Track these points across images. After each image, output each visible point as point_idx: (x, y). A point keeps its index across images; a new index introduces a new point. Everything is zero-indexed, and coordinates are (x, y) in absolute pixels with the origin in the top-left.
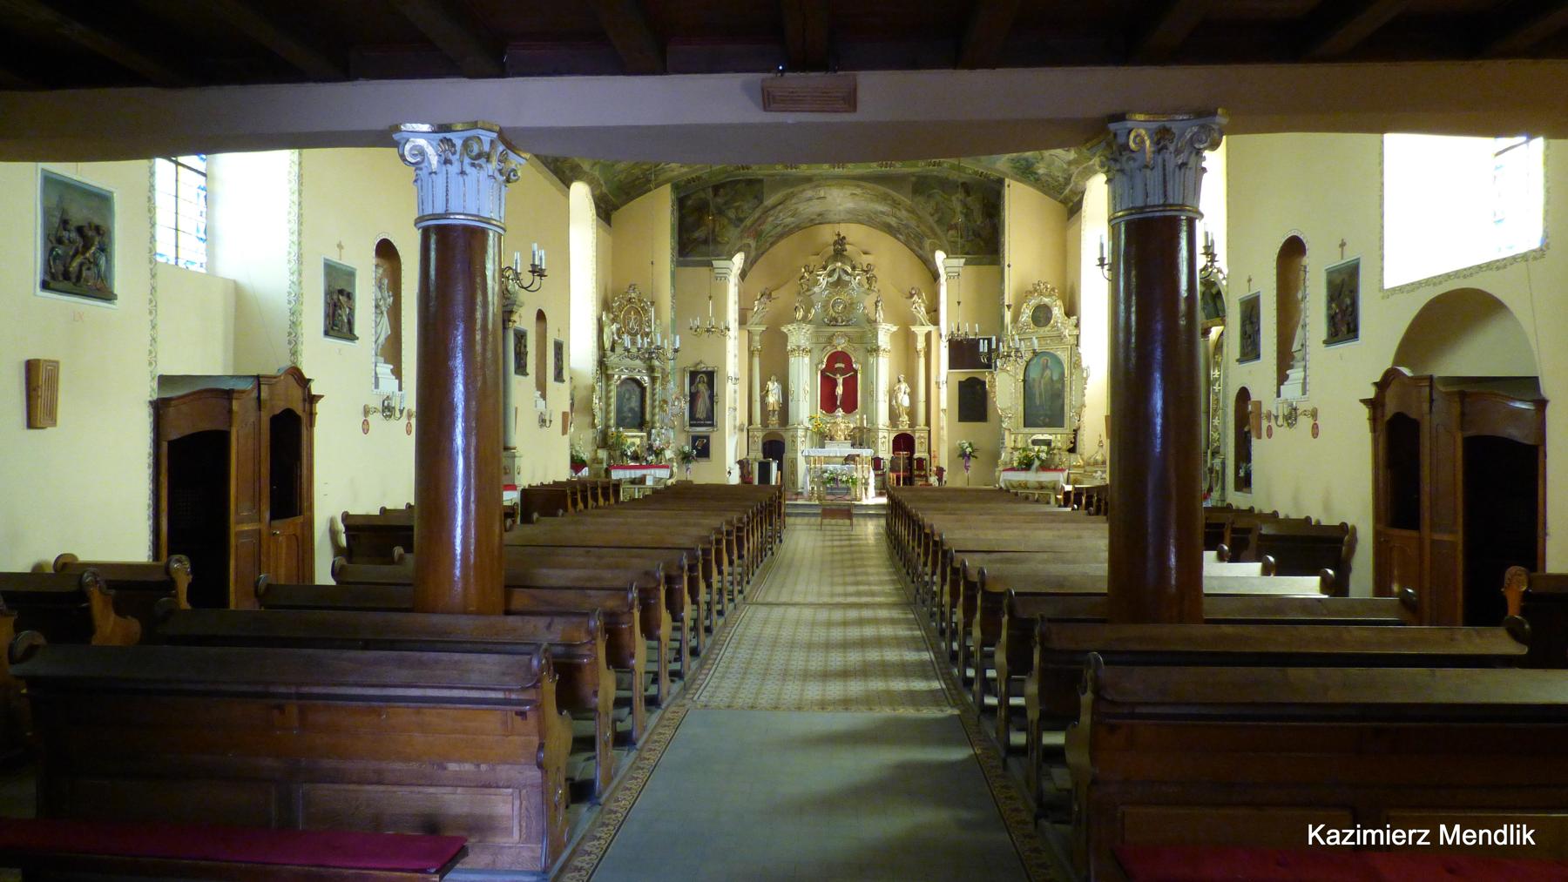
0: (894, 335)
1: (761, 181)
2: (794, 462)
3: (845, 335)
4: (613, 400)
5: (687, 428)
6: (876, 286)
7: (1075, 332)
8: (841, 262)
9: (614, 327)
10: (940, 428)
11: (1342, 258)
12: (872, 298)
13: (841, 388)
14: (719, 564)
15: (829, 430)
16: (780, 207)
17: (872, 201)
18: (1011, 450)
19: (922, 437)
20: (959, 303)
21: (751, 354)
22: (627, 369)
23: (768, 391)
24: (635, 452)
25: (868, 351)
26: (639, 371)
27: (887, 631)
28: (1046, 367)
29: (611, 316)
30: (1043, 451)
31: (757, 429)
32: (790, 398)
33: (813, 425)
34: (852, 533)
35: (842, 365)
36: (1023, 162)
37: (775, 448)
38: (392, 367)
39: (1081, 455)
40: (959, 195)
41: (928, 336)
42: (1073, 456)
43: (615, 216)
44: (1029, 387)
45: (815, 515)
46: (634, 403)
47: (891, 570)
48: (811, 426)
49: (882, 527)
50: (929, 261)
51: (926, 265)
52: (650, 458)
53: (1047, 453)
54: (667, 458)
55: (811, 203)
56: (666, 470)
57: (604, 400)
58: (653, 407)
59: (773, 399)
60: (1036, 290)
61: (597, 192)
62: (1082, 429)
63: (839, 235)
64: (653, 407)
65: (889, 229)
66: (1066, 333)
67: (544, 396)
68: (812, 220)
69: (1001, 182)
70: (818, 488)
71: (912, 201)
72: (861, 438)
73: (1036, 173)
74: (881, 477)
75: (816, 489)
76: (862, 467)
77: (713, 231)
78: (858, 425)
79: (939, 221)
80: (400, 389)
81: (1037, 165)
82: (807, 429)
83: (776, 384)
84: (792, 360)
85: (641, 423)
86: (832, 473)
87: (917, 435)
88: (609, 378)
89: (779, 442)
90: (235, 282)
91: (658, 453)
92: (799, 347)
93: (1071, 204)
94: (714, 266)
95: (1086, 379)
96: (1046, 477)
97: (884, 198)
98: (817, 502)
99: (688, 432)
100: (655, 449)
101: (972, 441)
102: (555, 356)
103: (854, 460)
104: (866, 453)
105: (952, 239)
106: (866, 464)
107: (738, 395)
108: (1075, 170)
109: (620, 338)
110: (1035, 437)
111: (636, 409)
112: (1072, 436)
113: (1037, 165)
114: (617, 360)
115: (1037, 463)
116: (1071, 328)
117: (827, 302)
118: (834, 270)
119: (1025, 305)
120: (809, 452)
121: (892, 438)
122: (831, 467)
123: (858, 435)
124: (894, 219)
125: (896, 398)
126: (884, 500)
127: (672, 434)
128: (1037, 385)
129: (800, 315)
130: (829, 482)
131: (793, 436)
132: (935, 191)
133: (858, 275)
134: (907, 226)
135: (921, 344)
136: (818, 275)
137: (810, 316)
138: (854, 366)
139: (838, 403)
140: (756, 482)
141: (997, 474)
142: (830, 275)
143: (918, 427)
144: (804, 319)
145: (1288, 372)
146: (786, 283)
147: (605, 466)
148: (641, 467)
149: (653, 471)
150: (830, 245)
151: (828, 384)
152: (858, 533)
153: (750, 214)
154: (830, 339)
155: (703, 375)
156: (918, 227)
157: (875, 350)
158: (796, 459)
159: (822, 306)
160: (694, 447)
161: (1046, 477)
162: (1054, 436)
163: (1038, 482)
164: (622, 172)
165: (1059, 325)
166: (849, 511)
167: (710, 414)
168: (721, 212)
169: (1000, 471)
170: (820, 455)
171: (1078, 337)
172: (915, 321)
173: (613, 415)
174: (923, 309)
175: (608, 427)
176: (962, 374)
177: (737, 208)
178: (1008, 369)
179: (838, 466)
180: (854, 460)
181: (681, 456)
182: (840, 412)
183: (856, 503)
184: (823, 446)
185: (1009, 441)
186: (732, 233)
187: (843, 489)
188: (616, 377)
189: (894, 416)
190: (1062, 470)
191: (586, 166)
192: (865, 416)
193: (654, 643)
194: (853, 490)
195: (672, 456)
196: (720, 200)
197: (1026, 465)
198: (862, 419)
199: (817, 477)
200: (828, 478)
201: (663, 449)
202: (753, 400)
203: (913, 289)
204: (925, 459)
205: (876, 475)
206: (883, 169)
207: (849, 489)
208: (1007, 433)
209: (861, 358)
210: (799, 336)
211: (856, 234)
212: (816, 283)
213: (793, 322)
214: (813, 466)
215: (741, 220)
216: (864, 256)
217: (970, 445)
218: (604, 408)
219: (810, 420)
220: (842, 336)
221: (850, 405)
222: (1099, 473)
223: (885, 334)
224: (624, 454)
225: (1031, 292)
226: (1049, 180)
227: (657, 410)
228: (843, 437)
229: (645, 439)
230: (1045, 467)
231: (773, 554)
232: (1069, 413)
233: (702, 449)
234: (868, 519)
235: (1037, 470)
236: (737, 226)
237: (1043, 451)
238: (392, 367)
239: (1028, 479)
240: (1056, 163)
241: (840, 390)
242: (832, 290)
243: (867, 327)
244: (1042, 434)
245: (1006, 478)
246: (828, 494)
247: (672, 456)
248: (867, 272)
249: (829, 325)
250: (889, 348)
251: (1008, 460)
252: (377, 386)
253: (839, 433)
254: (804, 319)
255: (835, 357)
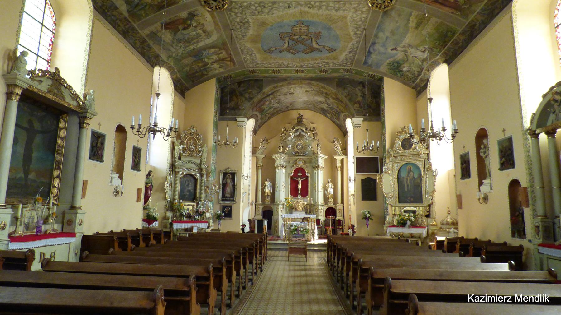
0: (326, 161)
1: (262, 80)
2: (277, 221)
3: (303, 160)
4: (178, 185)
5: (221, 202)
6: (317, 138)
7: (427, 151)
8: (301, 126)
9: (181, 147)
10: (349, 205)
11: (504, 136)
12: (316, 143)
13: (300, 185)
14: (244, 264)
15: (295, 205)
16: (271, 96)
17: (315, 95)
18: (392, 216)
19: (340, 209)
20: (367, 130)
21: (258, 168)
22: (187, 169)
23: (265, 186)
24: (189, 213)
25: (313, 168)
26: (194, 171)
27: (321, 296)
28: (410, 171)
29: (180, 141)
30: (411, 216)
31: (260, 204)
32: (276, 189)
33: (286, 202)
34: (307, 263)
35: (301, 174)
36: (396, 64)
37: (268, 214)
38: (118, 175)
39: (434, 218)
40: (359, 88)
41: (342, 161)
42: (429, 219)
43: (187, 93)
44: (401, 182)
45: (286, 250)
46: (191, 188)
47: (328, 281)
48: (285, 203)
49: (324, 259)
50: (342, 126)
51: (340, 129)
52: (197, 217)
53: (414, 217)
54: (207, 217)
55: (286, 96)
56: (206, 223)
57: (173, 185)
58: (201, 190)
59: (267, 190)
60: (403, 131)
61: (174, 77)
62: (434, 204)
63: (300, 114)
64: (201, 190)
65: (323, 112)
66: (422, 152)
67: (121, 177)
68: (287, 107)
69: (381, 80)
70: (288, 234)
71: (336, 90)
72: (310, 209)
73: (402, 71)
74: (320, 229)
75: (287, 235)
76: (311, 224)
77: (237, 103)
78: (309, 203)
79: (350, 100)
80: (122, 184)
81: (403, 65)
82: (284, 204)
83: (269, 183)
84: (277, 171)
85: (193, 198)
86: (295, 227)
87: (337, 208)
88: (176, 173)
89: (271, 211)
90: (154, 167)
91: (202, 214)
92: (280, 165)
93: (419, 88)
94: (237, 120)
95: (435, 176)
96: (414, 231)
97: (320, 93)
98: (287, 242)
99: (221, 204)
100: (199, 212)
101: (370, 211)
102: (133, 155)
103: (307, 220)
104: (313, 216)
105: (357, 108)
106: (313, 222)
107: (251, 187)
108: (425, 65)
109: (184, 153)
110: (405, 209)
111: (192, 191)
112: (428, 208)
113: (403, 65)
114: (181, 164)
115: (409, 223)
116: (424, 150)
117: (294, 145)
118: (298, 130)
119: (397, 139)
120: (284, 216)
121: (325, 209)
122: (295, 223)
123: (308, 208)
124: (326, 105)
125: (327, 190)
126: (325, 241)
127: (211, 204)
128: (405, 180)
129: (281, 150)
130: (294, 231)
131: (277, 208)
132: (348, 85)
133: (309, 132)
134: (332, 108)
135: (339, 165)
136: (290, 132)
137: (286, 151)
138: (307, 174)
139: (299, 192)
140: (256, 232)
141: (385, 228)
142: (295, 132)
143: (338, 204)
144: (283, 152)
145: (483, 181)
146: (275, 136)
147: (170, 221)
148: (192, 222)
149: (198, 224)
150: (295, 119)
151: (294, 183)
152: (311, 264)
153: (256, 95)
154: (295, 162)
155: (230, 175)
156: (338, 107)
157: (317, 167)
158: (278, 219)
159: (292, 147)
160: (223, 212)
161: (414, 231)
162: (418, 208)
163: (410, 233)
164: (187, 65)
165: (417, 148)
166: (305, 248)
167: (232, 194)
168: (241, 95)
169: (387, 227)
170: (289, 217)
171: (428, 154)
172: (336, 153)
173: (177, 193)
174: (340, 148)
175: (174, 199)
176: (363, 176)
177: (250, 93)
178: (389, 172)
179: (299, 223)
180: (307, 220)
181: (216, 216)
182: (300, 197)
183: (308, 243)
184: (291, 213)
185: (391, 211)
186: (247, 105)
187: (301, 234)
188: (181, 173)
189: (326, 199)
190: (424, 227)
191: (164, 57)
192: (312, 199)
193: (220, 293)
194: (306, 236)
195: (210, 216)
196: (241, 89)
197: (402, 224)
198: (310, 200)
199: (288, 228)
200: (293, 229)
201: (204, 212)
202: (258, 190)
203: (334, 138)
204: (342, 220)
205: (318, 228)
206: (322, 73)
207: (304, 235)
208: (389, 206)
209: (310, 171)
210: (280, 160)
211: (308, 115)
212: (289, 136)
213: (278, 153)
214: (286, 223)
215: (251, 98)
216: (311, 124)
217: (369, 212)
218: (173, 189)
219: (285, 200)
220: (301, 160)
221: (305, 193)
222: (453, 229)
223: (322, 160)
224: (181, 215)
225: (400, 132)
226: (409, 74)
227: (203, 191)
228: (301, 209)
229: (195, 207)
230: (413, 225)
231: (252, 284)
232: (425, 195)
233: (227, 213)
234: (315, 252)
235: (409, 227)
236: (249, 102)
237: (411, 216)
238: (118, 175)
239: (404, 232)
240: (416, 62)
241: (300, 186)
242: (296, 139)
243: (313, 156)
244: (410, 207)
245: (391, 232)
246: (294, 237)
247: (210, 216)
248: (313, 131)
249: (294, 155)
250: (324, 166)
251: (391, 221)
252: (111, 182)
253: (300, 207)
254: (283, 152)
255: (298, 170)
